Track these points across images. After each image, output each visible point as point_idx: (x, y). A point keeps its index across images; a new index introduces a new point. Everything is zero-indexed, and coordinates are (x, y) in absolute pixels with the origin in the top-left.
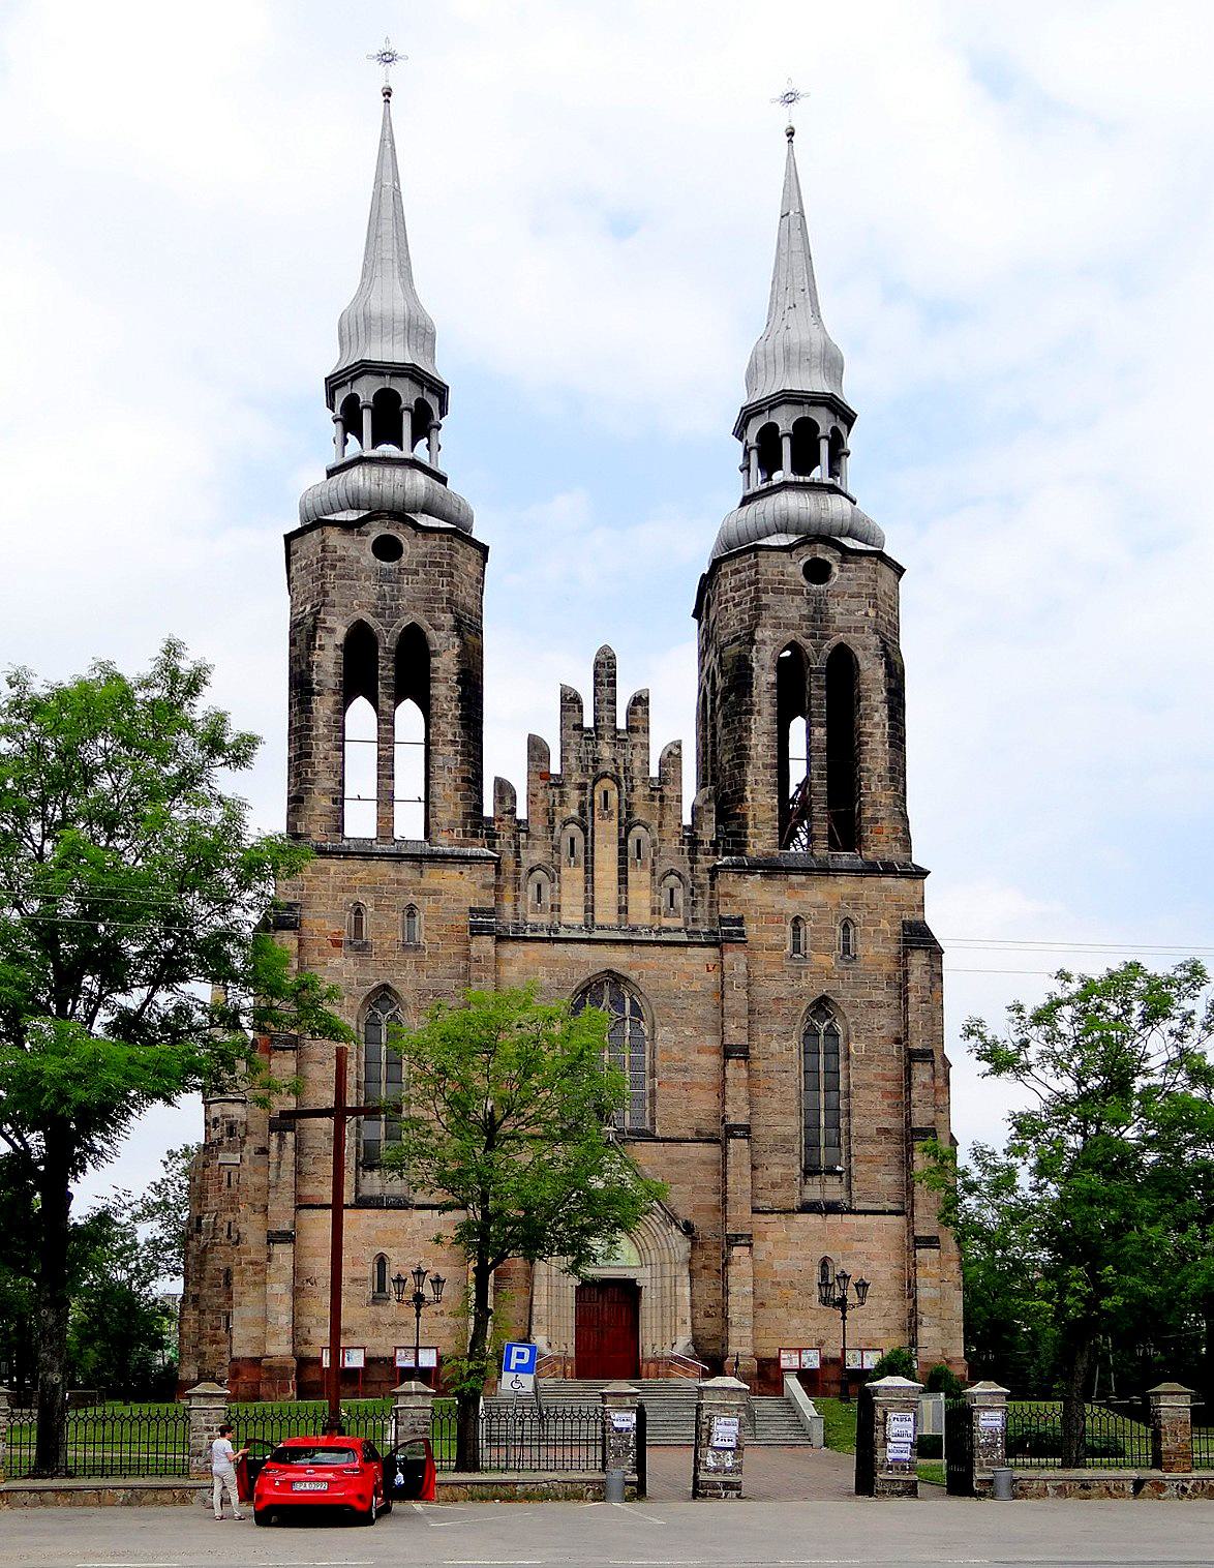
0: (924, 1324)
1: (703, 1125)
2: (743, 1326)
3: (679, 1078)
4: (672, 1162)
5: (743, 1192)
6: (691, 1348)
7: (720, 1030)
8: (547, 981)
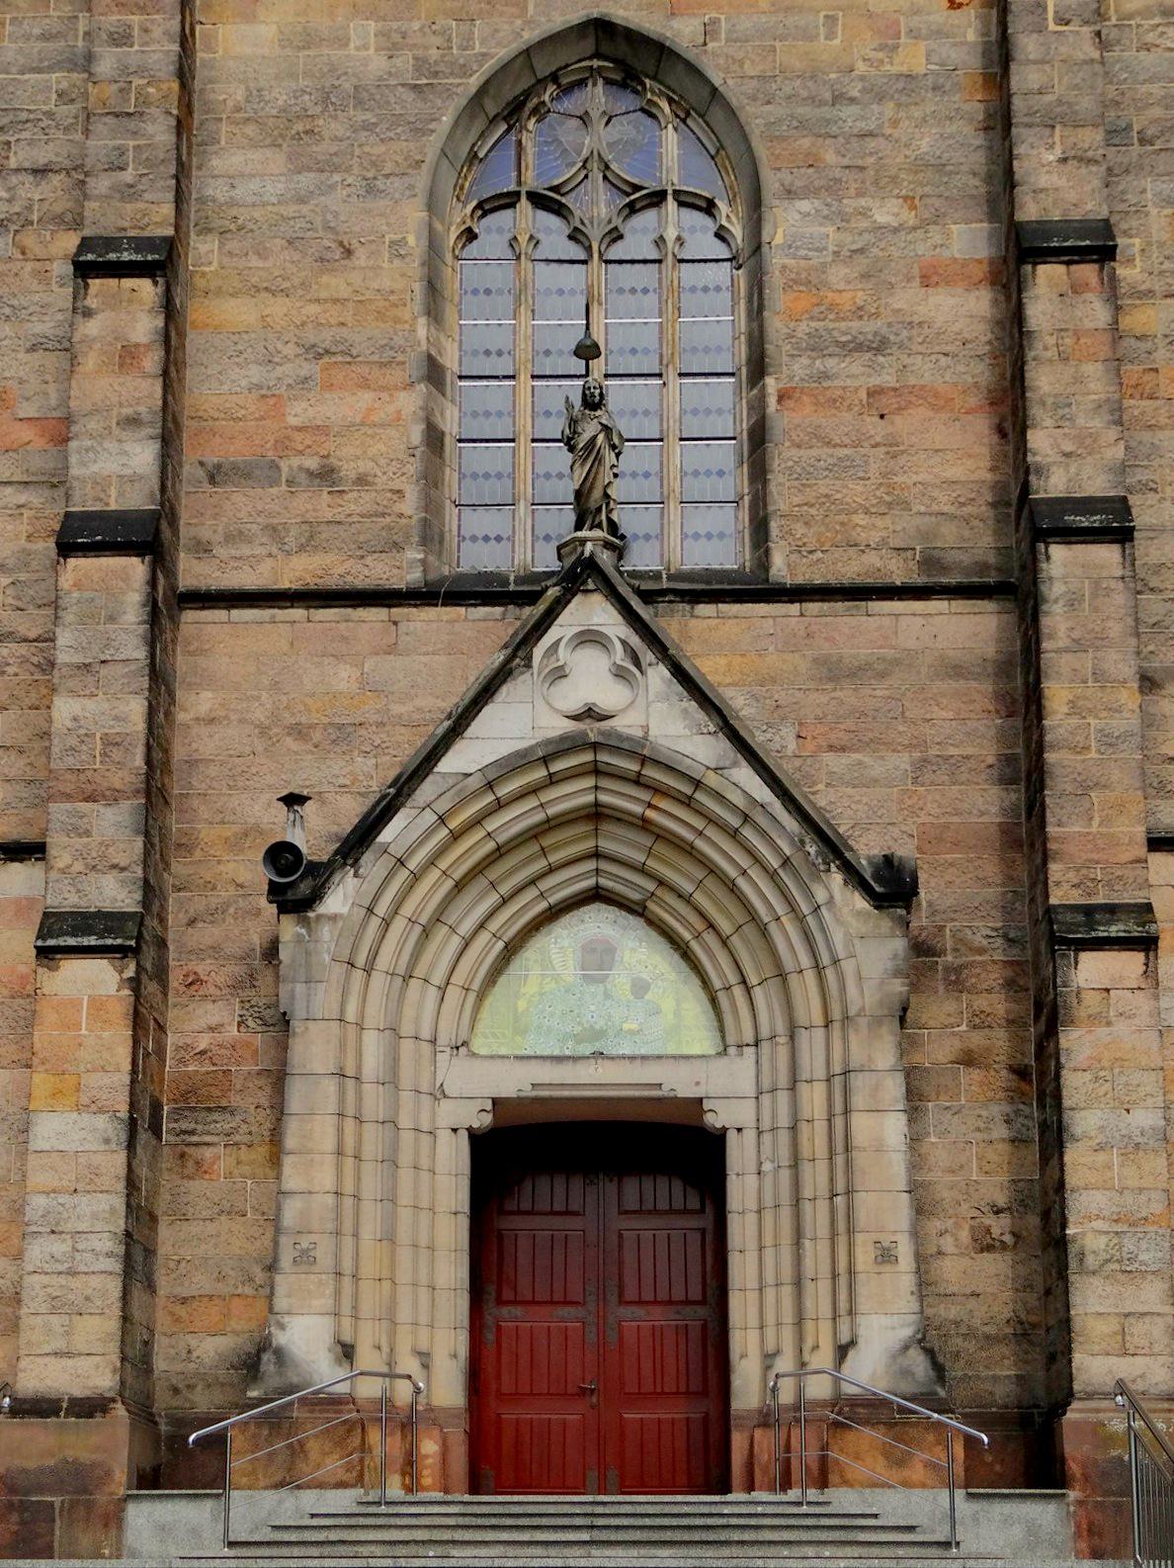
1: (949, 535)
2: (1129, 1271)
3: (854, 374)
4: (834, 672)
5: (1109, 741)
6: (919, 1363)
7: (1003, 182)
8: (378, 64)
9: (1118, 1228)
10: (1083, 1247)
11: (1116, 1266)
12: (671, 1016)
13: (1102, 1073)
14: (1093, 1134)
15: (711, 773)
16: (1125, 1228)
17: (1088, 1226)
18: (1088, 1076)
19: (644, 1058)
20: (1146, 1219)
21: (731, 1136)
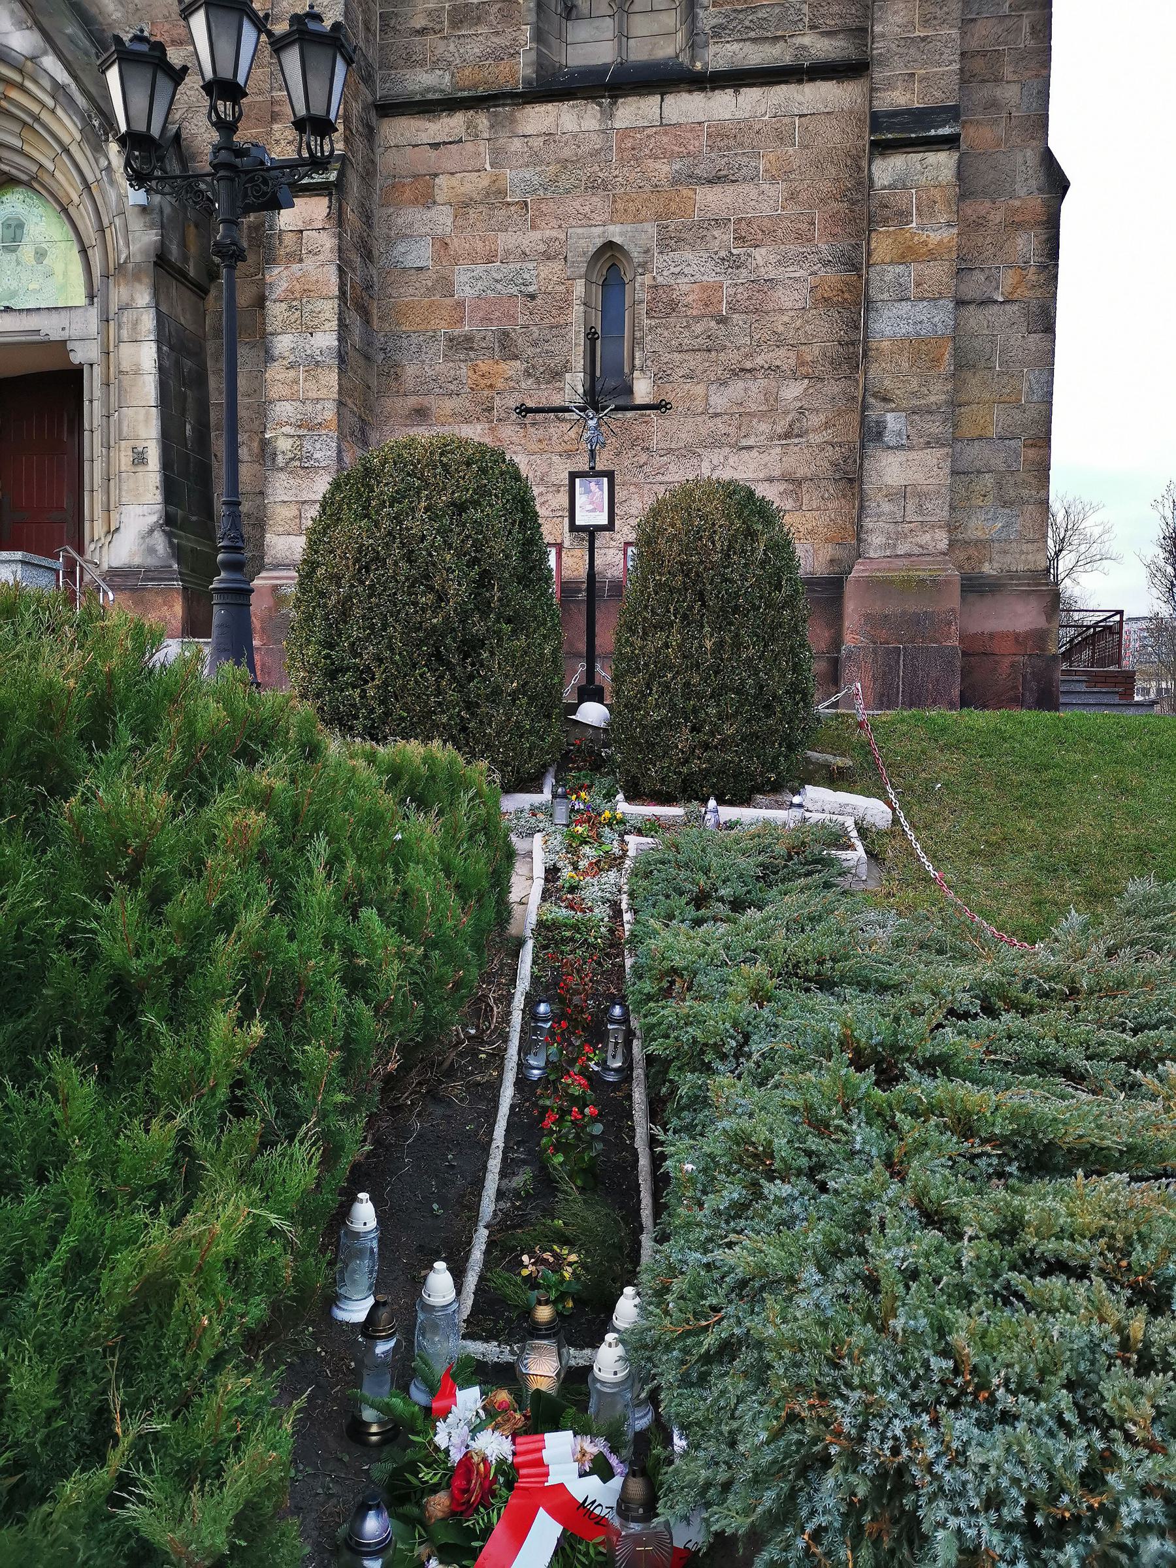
0: (889, 439)
9: (301, 432)
10: (275, 448)
11: (297, 463)
12: (61, 277)
13: (294, 303)
14: (286, 354)
15: (29, 63)
16: (305, 432)
17: (279, 431)
18: (284, 305)
19: (28, 310)
20: (320, 424)
21: (86, 369)
